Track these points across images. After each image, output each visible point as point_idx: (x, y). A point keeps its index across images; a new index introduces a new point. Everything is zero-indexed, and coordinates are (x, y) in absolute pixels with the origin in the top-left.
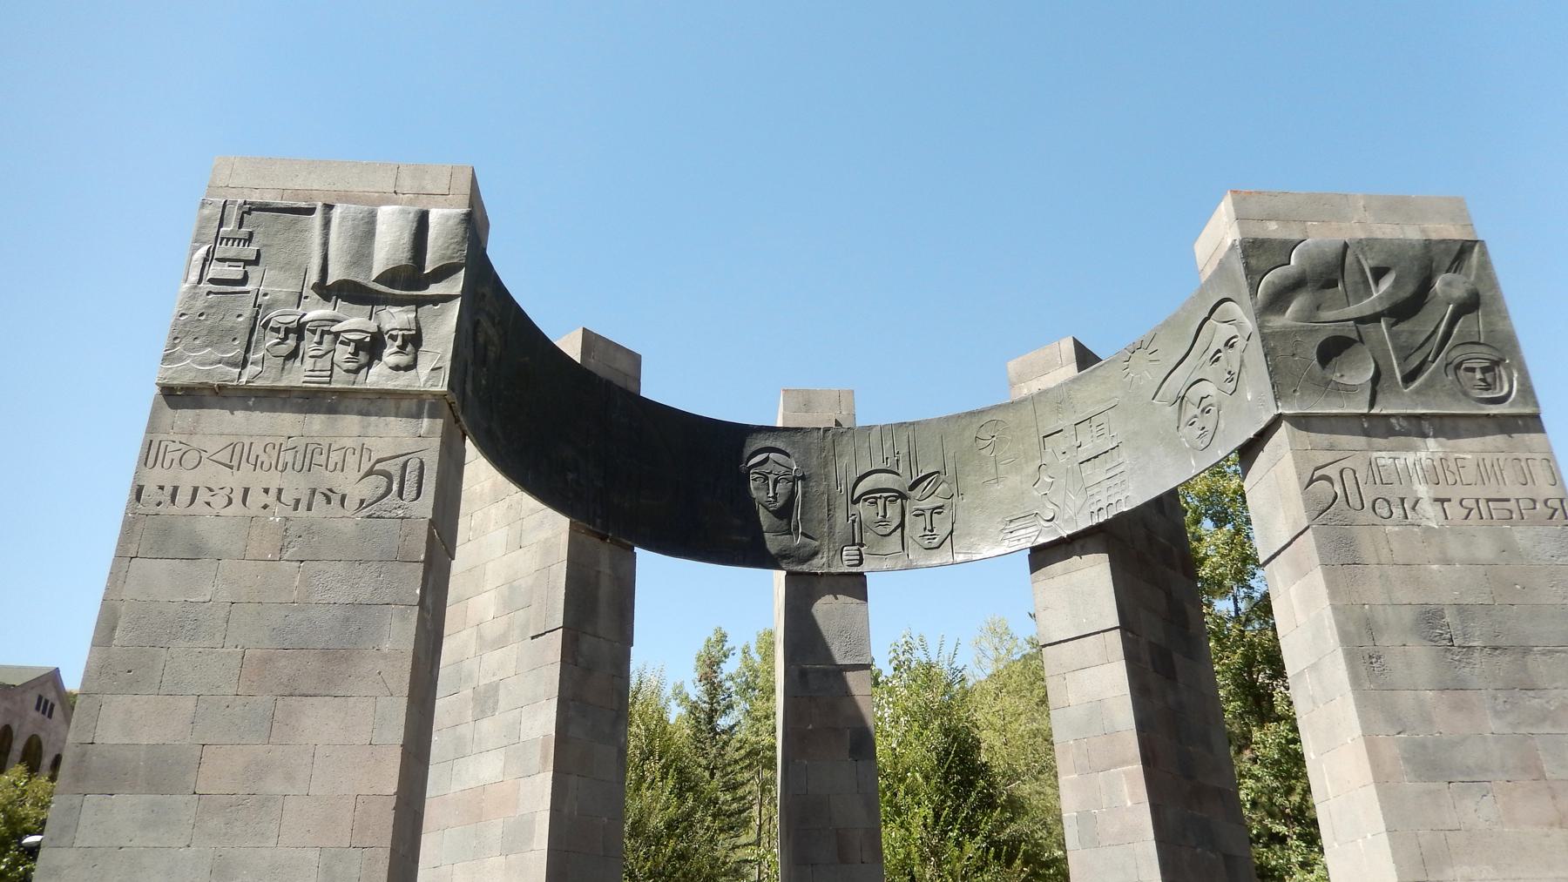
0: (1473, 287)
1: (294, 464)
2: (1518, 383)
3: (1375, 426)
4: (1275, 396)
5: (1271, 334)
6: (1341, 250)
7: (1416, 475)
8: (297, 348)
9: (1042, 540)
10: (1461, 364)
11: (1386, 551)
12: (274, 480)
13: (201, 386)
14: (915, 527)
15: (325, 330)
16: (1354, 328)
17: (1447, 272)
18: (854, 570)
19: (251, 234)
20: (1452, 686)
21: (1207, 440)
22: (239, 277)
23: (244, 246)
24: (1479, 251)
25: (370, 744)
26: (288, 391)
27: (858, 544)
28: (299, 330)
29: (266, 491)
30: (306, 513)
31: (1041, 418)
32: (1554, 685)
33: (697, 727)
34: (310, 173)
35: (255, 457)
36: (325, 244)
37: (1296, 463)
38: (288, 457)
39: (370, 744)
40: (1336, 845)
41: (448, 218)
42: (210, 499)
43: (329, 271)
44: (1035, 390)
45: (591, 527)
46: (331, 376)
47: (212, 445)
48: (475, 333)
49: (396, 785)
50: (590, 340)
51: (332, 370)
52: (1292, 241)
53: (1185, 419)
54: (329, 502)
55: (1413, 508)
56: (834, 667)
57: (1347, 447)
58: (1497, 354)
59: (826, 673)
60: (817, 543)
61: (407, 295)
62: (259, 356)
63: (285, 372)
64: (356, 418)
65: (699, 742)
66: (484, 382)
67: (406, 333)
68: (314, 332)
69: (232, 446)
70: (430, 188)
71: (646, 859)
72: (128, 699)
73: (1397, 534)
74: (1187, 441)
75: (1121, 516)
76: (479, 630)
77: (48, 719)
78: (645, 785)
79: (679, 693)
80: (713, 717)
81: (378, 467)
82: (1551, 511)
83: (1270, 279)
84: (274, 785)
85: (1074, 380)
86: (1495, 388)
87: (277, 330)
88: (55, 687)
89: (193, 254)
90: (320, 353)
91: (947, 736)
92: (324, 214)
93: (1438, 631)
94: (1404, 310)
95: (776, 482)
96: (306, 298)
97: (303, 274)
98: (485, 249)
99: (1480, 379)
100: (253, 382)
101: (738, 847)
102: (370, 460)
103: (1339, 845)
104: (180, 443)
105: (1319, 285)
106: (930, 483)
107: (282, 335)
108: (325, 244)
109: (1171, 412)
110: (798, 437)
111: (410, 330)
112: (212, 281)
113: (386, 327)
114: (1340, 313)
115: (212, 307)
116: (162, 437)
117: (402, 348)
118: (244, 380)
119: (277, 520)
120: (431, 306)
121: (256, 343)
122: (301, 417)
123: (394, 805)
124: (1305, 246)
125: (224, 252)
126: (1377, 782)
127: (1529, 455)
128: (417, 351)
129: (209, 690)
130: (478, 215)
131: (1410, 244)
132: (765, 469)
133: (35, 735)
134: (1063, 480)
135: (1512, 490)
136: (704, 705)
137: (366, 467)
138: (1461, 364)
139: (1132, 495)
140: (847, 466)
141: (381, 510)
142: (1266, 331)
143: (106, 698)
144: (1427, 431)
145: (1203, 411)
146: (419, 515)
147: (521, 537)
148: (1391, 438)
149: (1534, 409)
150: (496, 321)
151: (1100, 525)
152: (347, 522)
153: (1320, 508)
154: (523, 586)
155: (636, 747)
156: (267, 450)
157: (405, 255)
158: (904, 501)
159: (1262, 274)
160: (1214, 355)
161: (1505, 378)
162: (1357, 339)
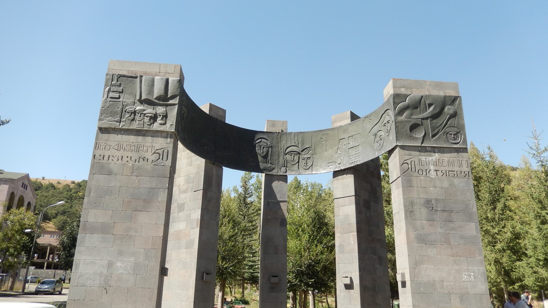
0: (455, 110)
3: (422, 149)
5: (398, 122)
8: (134, 118)
9: (336, 170)
10: (448, 132)
12: (130, 154)
14: (302, 163)
15: (141, 112)
17: (449, 105)
18: (284, 174)
20: (431, 220)
22: (118, 97)
26: (132, 130)
27: (286, 167)
28: (135, 113)
29: (128, 157)
32: (458, 221)
33: (240, 202)
34: (136, 66)
36: (141, 88)
41: (174, 81)
42: (113, 159)
43: (142, 96)
44: (338, 126)
46: (143, 126)
47: (113, 144)
48: (181, 111)
49: (163, 233)
50: (212, 106)
51: (144, 124)
52: (407, 95)
54: (144, 161)
55: (429, 172)
56: (277, 201)
58: (459, 130)
59: (275, 203)
60: (274, 166)
62: (124, 119)
63: (131, 124)
64: (150, 138)
67: (163, 114)
68: (139, 113)
70: (169, 71)
71: (223, 247)
73: (423, 179)
80: (245, 199)
81: (156, 151)
85: (349, 124)
87: (129, 112)
88: (28, 180)
90: (141, 119)
92: (140, 79)
94: (435, 116)
96: (136, 103)
105: (413, 108)
107: (130, 114)
108: (141, 88)
109: (373, 137)
110: (270, 135)
111: (164, 113)
112: (110, 98)
113: (158, 112)
114: (418, 116)
115: (111, 105)
116: (100, 141)
117: (162, 119)
118: (120, 126)
119: (131, 165)
121: (123, 116)
122: (136, 137)
125: (114, 89)
126: (408, 243)
127: (462, 159)
128: (166, 119)
132: (260, 144)
133: (22, 195)
135: (456, 168)
136: (242, 195)
137: (153, 151)
138: (448, 132)
139: (360, 160)
140: (284, 144)
142: (396, 121)
144: (436, 151)
145: (380, 139)
146: (167, 165)
148: (426, 153)
150: (186, 106)
151: (352, 167)
154: (192, 177)
157: (163, 92)
160: (385, 124)
162: (421, 124)
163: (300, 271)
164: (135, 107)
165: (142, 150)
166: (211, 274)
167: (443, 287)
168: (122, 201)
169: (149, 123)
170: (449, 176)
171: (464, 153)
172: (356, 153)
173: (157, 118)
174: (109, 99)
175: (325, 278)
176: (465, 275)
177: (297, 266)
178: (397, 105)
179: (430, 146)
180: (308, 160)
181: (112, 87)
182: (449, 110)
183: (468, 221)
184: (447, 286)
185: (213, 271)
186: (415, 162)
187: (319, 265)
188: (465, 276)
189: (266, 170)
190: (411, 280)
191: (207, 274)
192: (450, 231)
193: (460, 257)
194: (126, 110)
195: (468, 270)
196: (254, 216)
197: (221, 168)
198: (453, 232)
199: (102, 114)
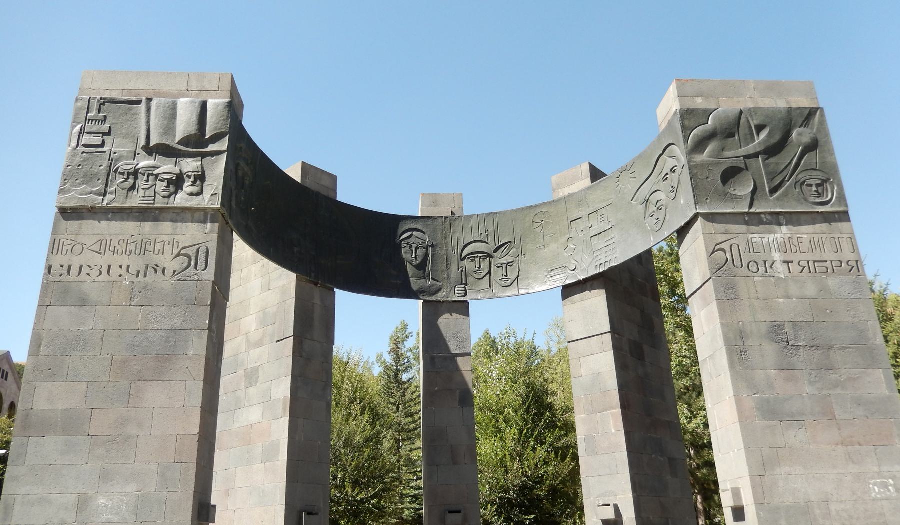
0: (815, 136)
1: (135, 251)
2: (837, 193)
3: (752, 219)
4: (695, 202)
5: (695, 165)
6: (738, 114)
7: (774, 247)
8: (134, 184)
9: (568, 282)
10: (804, 182)
11: (754, 291)
12: (125, 260)
13: (81, 207)
14: (497, 274)
15: (150, 173)
16: (743, 161)
18: (462, 299)
19: (105, 117)
20: (786, 367)
21: (660, 225)
22: (100, 143)
23: (102, 124)
24: (820, 114)
25: (184, 406)
27: (464, 284)
28: (135, 173)
29: (121, 266)
30: (143, 279)
31: (569, 210)
32: (845, 367)
34: (138, 79)
35: (114, 247)
36: (148, 122)
37: (705, 241)
38: (132, 247)
39: (184, 406)
40: (720, 454)
41: (218, 105)
42: (90, 272)
43: (151, 138)
44: (567, 194)
45: (309, 278)
46: (154, 200)
47: (89, 241)
50: (306, 169)
51: (155, 196)
52: (710, 110)
53: (648, 213)
54: (156, 271)
55: (771, 267)
57: (735, 232)
59: (445, 358)
60: (440, 284)
61: (196, 152)
62: (113, 189)
63: (129, 198)
64: (169, 224)
65: (390, 389)
66: (243, 198)
67: (196, 174)
68: (144, 174)
69: (100, 241)
70: (208, 87)
72: (49, 384)
74: (649, 226)
75: (612, 269)
76: (247, 336)
77: (5, 381)
78: (352, 418)
79: (380, 359)
80: (398, 374)
82: (850, 267)
83: (697, 133)
84: (132, 430)
85: (589, 188)
86: (824, 196)
87: (123, 174)
89: (73, 130)
90: (148, 186)
91: (528, 387)
93: (780, 336)
94: (772, 150)
95: (417, 249)
96: (139, 154)
97: (136, 140)
98: (241, 121)
99: (815, 191)
100: (110, 204)
101: (414, 449)
102: (178, 248)
103: (722, 455)
104: (71, 240)
106: (506, 248)
107: (126, 177)
108: (148, 122)
109: (641, 208)
110: (430, 222)
111: (198, 172)
112: (85, 146)
113: (185, 171)
114: (736, 152)
116: (61, 237)
117: (194, 183)
118: (105, 203)
119: (128, 283)
120: (210, 157)
123: (198, 439)
124: (717, 113)
126: (741, 421)
127: (840, 235)
128: (203, 184)
129: (94, 379)
130: (236, 100)
131: (779, 110)
132: (410, 241)
134: (581, 247)
135: (829, 255)
137: (176, 252)
138: (804, 182)
140: (458, 238)
141: (185, 276)
142: (692, 164)
143: (37, 384)
145: (658, 208)
147: (269, 284)
148: (761, 226)
149: (845, 208)
150: (249, 162)
152: (166, 283)
153: (717, 267)
155: (346, 396)
156: (120, 243)
157: (194, 128)
158: (491, 259)
159: (691, 130)
161: (830, 190)
162: (745, 168)
163: (505, 499)
164: (138, 163)
165: (153, 251)
166: (316, 514)
167: (830, 514)
168: (110, 360)
169: (166, 194)
170: (816, 272)
171: (843, 223)
172: (607, 244)
173: (184, 181)
174: (81, 149)
175: (556, 511)
176: (875, 484)
177: (500, 489)
178: (689, 132)
179: (769, 210)
180: (508, 267)
181: (88, 123)
182: (800, 136)
183: (869, 366)
185: (322, 505)
186: (739, 247)
187: (541, 486)
188: (876, 487)
189: (424, 292)
190: (756, 503)
191: (309, 513)
192: (830, 389)
193: (860, 445)
194: (118, 169)
195: (879, 474)
196: (415, 404)
197: (331, 292)
198: (838, 390)
199: (66, 180)
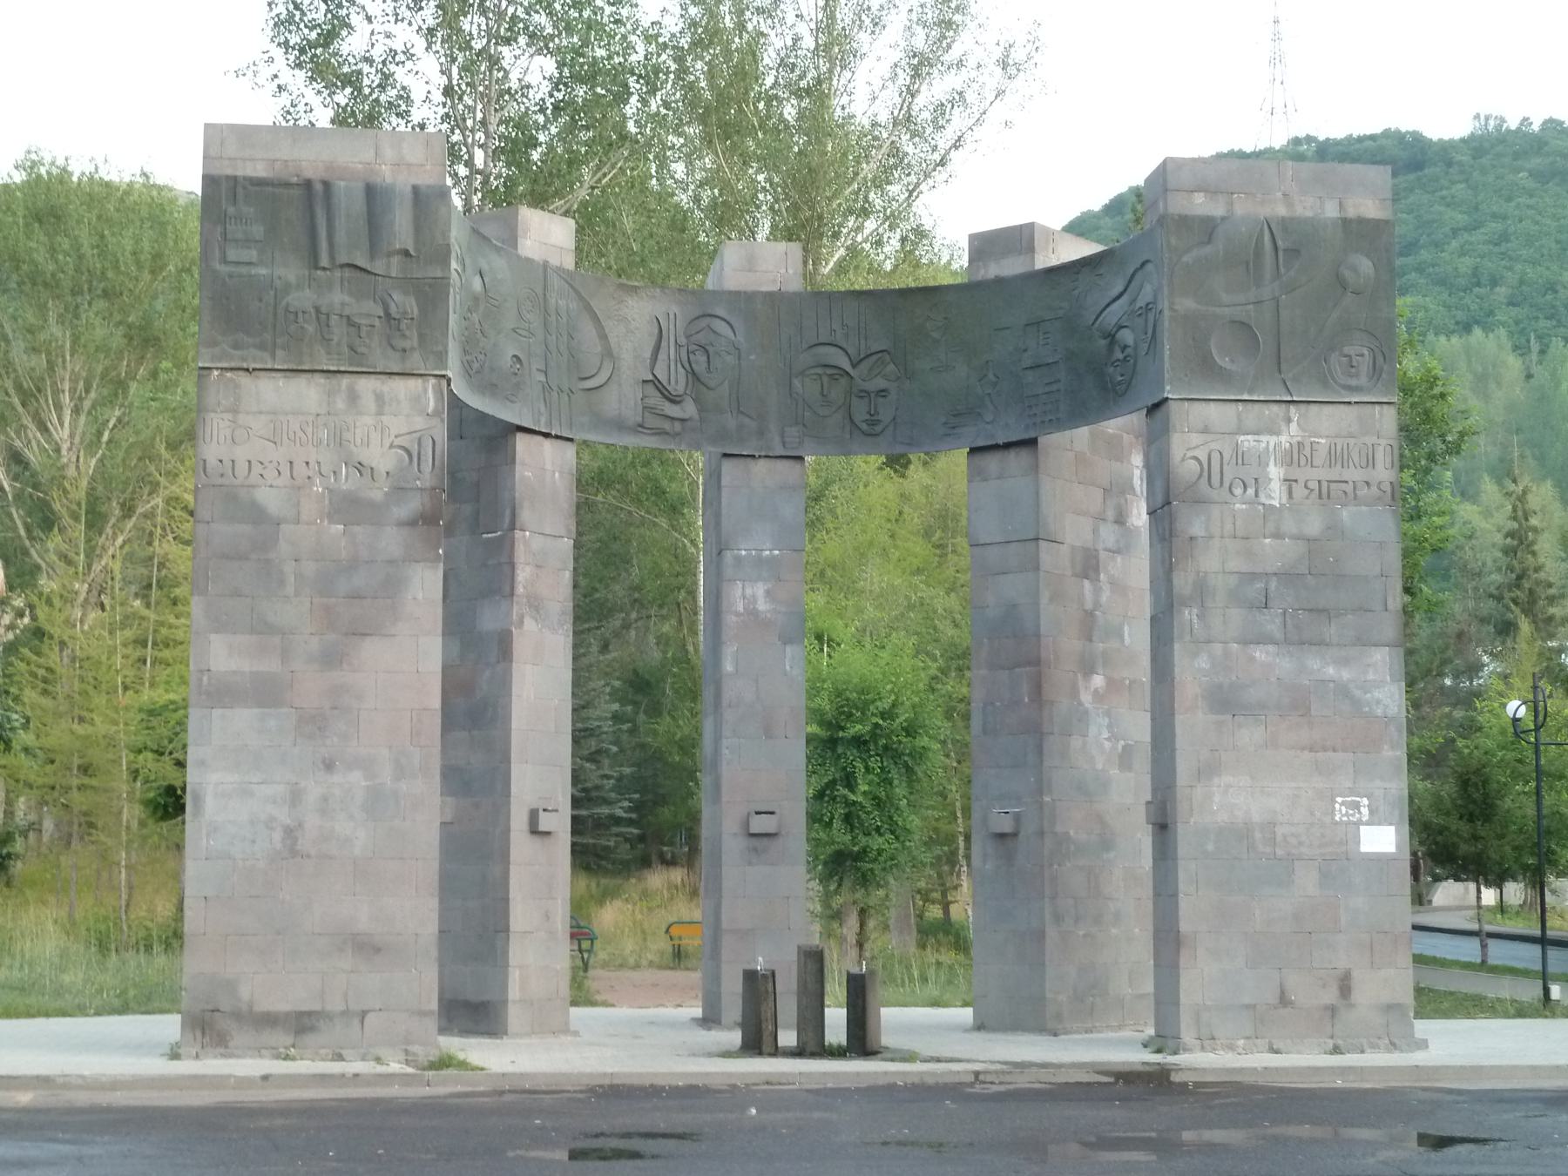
184: (1285, 837)
188: (1343, 809)
